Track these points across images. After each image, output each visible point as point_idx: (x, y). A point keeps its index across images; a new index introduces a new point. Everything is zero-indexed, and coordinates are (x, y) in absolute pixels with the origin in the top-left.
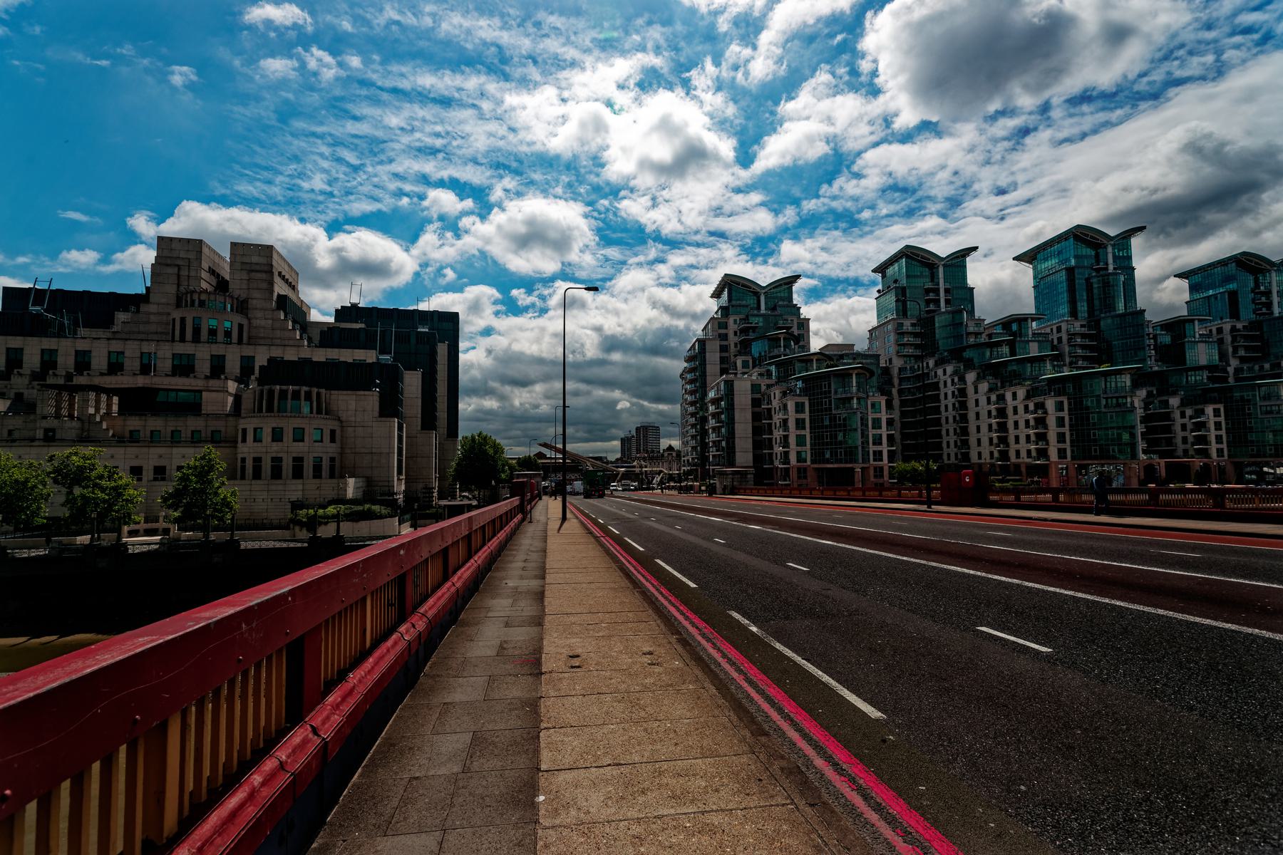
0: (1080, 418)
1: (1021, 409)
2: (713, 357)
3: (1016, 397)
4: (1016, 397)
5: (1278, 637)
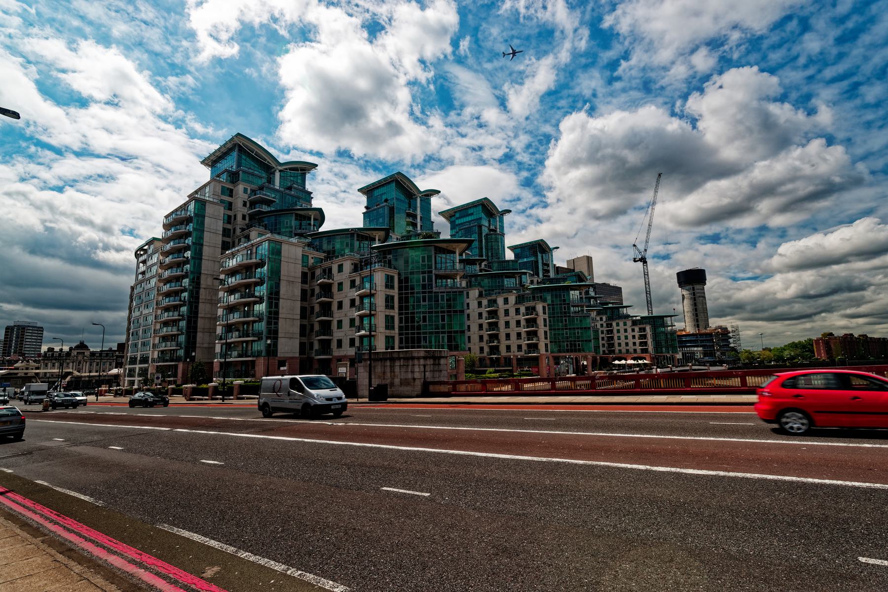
1: (512, 312)
2: (214, 224)
3: (507, 303)
4: (507, 303)
5: (886, 563)
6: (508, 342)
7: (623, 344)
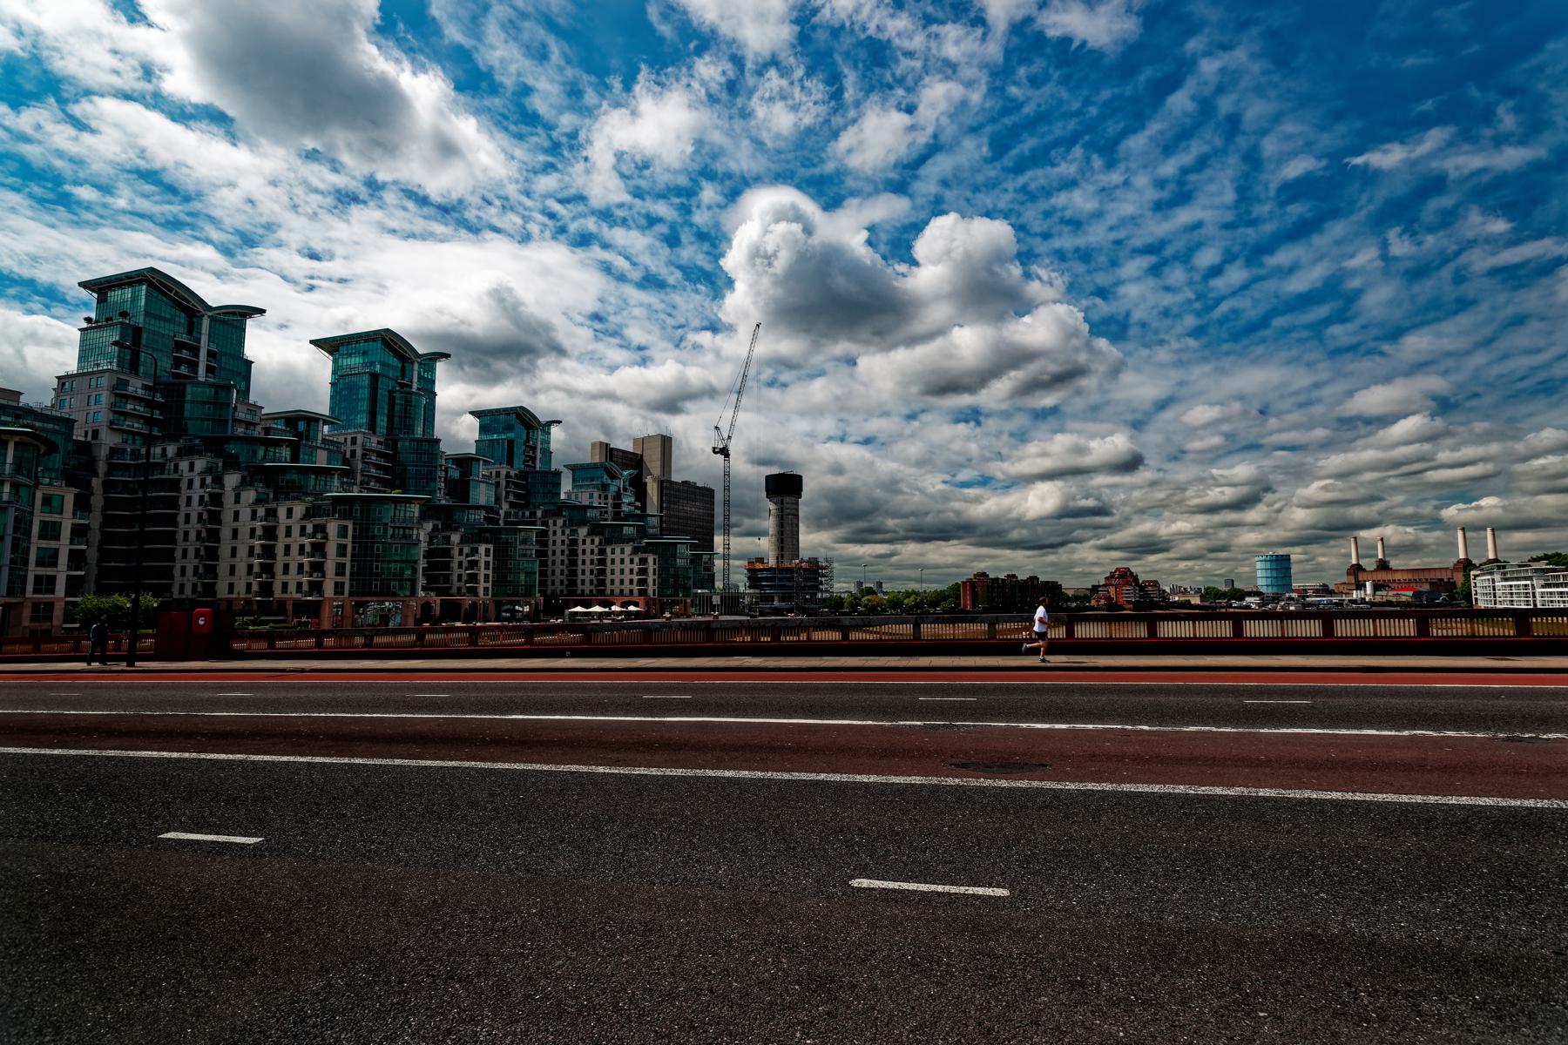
0: (365, 551)
6: (285, 578)
7: (617, 582)
